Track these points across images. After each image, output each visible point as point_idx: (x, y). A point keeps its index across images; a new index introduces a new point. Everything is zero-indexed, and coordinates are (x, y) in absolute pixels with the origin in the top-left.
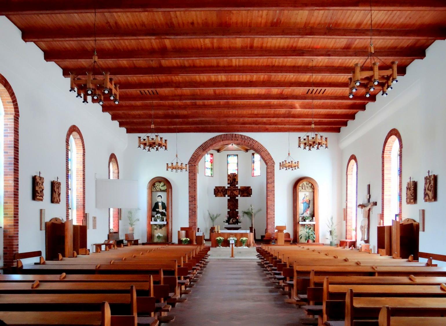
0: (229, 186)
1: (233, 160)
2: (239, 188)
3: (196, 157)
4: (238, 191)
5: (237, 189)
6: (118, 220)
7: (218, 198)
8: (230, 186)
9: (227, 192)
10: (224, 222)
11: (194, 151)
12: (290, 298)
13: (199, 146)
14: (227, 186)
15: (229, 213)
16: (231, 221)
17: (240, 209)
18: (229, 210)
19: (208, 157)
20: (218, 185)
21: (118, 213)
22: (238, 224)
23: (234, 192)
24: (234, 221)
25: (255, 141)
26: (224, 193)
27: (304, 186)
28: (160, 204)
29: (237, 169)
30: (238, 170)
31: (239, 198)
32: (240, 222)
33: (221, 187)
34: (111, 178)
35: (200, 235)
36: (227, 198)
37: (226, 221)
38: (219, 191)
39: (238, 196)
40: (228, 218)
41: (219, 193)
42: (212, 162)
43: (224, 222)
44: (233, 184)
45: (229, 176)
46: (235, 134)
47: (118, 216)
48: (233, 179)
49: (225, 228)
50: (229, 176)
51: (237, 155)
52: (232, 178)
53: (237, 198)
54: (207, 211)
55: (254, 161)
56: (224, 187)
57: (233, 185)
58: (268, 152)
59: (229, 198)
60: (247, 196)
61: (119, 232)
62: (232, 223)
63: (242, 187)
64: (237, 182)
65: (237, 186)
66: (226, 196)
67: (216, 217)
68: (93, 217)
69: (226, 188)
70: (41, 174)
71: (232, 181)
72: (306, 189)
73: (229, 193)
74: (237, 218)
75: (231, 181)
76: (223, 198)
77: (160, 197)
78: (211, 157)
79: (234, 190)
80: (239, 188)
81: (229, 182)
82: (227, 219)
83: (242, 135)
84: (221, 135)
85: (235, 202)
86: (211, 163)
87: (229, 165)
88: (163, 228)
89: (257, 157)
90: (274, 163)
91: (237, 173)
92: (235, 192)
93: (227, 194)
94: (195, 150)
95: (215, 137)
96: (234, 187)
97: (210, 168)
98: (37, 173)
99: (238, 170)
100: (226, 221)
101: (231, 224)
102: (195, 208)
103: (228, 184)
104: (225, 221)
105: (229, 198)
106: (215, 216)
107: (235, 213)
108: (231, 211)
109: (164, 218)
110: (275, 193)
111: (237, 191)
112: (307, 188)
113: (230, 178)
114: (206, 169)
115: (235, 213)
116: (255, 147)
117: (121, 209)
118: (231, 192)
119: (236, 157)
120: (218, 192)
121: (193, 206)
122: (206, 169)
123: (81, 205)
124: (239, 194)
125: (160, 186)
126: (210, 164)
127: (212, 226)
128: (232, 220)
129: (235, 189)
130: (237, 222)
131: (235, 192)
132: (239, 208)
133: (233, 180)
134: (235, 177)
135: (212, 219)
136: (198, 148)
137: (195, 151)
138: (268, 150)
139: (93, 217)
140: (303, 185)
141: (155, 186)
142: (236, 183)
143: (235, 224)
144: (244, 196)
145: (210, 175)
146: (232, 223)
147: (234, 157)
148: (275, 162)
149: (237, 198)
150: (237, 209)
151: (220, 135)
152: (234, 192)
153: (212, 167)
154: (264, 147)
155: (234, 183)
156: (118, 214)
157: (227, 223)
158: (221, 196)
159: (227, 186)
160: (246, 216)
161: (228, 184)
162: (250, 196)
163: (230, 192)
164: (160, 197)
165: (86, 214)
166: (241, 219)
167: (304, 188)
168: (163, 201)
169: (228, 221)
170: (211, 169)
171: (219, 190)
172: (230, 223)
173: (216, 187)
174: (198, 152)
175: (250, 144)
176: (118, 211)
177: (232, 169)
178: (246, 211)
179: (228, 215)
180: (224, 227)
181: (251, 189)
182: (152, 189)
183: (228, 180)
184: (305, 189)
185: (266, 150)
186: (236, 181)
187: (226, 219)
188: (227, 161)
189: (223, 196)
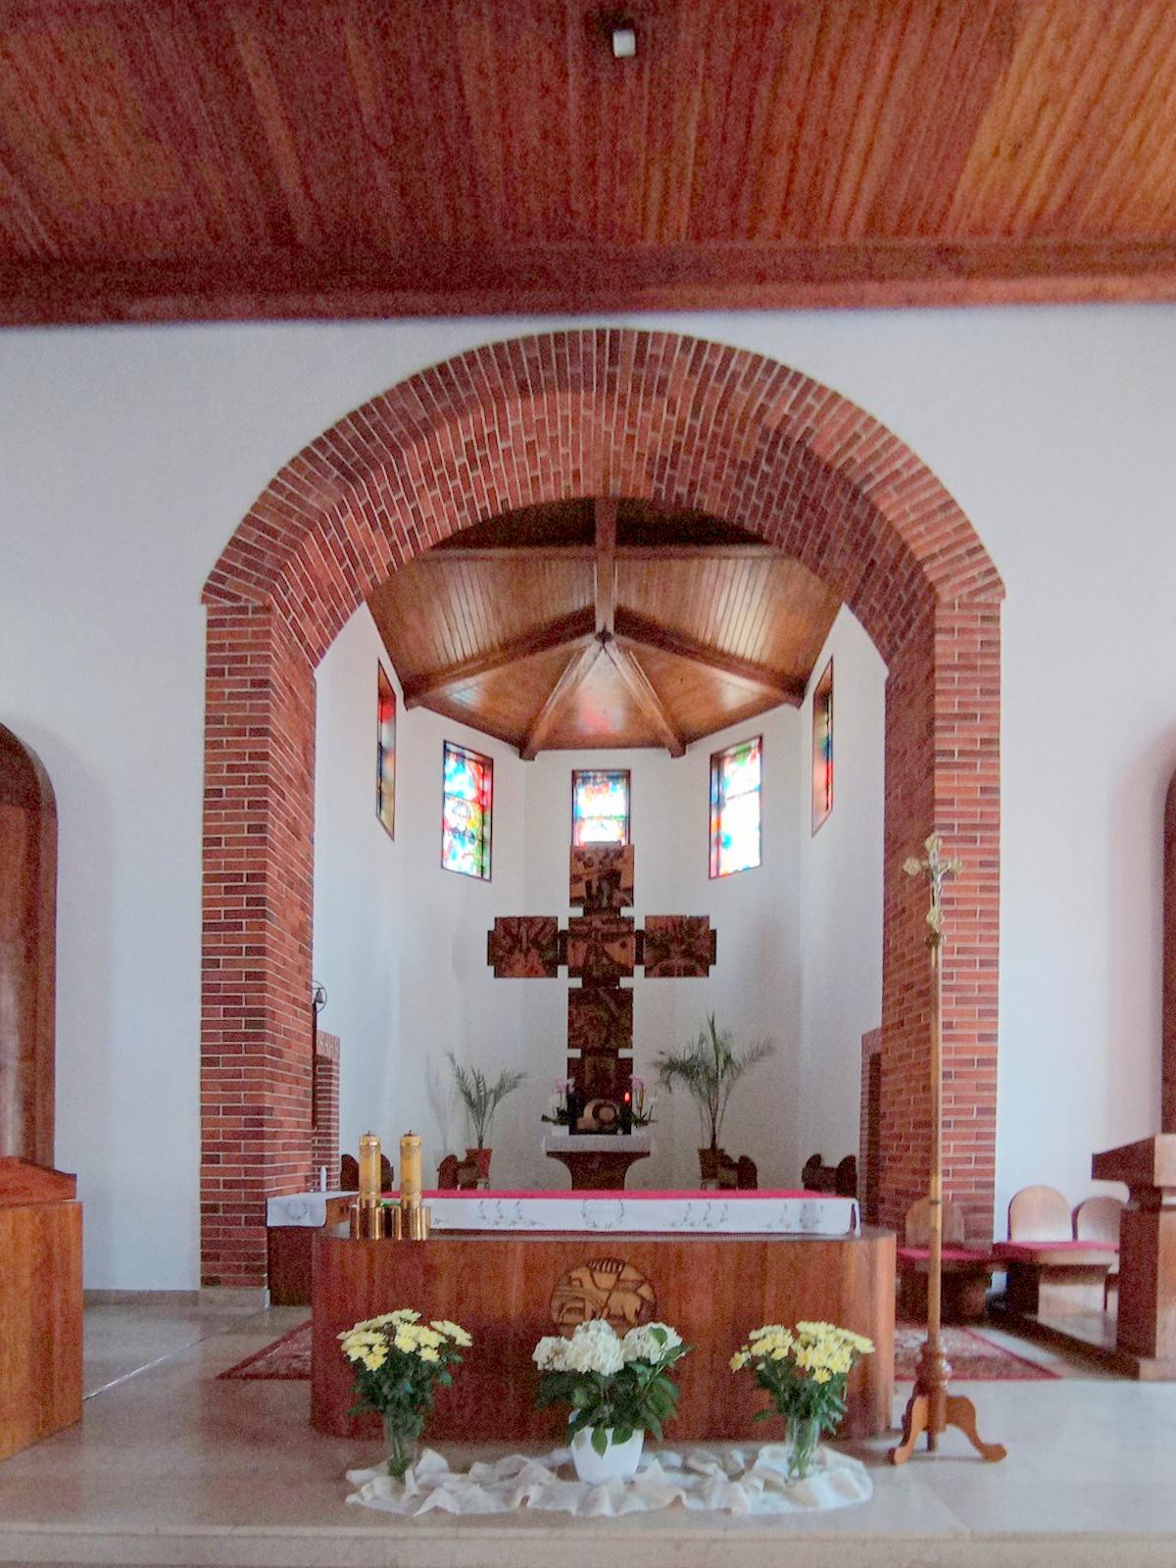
2: (639, 925)
3: (274, 533)
4: (632, 942)
5: (624, 928)
7: (517, 988)
8: (587, 912)
9: (564, 951)
10: (545, 1118)
11: (262, 486)
13: (305, 441)
14: (565, 914)
15: (574, 1067)
16: (588, 1111)
17: (643, 1051)
18: (577, 1053)
20: (516, 910)
22: (627, 1131)
23: (608, 947)
24: (607, 1114)
25: (822, 389)
26: (550, 955)
31: (638, 983)
32: (642, 1122)
33: (531, 921)
35: (306, 1222)
36: (565, 982)
37: (561, 1113)
39: (630, 973)
40: (570, 1099)
42: (485, 804)
43: (545, 1118)
44: (605, 902)
45: (578, 855)
46: (643, 337)
50: (578, 855)
52: (597, 866)
53: (625, 982)
54: (447, 1060)
57: (599, 910)
58: (944, 492)
59: (577, 983)
60: (690, 972)
62: (594, 1125)
63: (656, 918)
64: (630, 890)
65: (625, 912)
66: (563, 970)
67: (498, 1093)
71: (599, 888)
73: (578, 953)
74: (627, 1096)
75: (589, 885)
76: (540, 984)
78: (483, 776)
80: (639, 925)
81: (581, 889)
82: (564, 1106)
83: (702, 344)
84: (513, 345)
85: (613, 1006)
86: (483, 808)
90: (998, 582)
91: (624, 842)
92: (614, 950)
93: (564, 963)
94: (273, 474)
95: (456, 361)
97: (477, 834)
100: (561, 1113)
101: (588, 1132)
104: (554, 1115)
105: (577, 983)
106: (492, 1083)
107: (612, 1073)
110: (1004, 846)
111: (624, 945)
113: (586, 865)
115: (612, 1073)
116: (818, 449)
120: (510, 951)
121: (244, 964)
124: (639, 961)
126: (475, 812)
127: (475, 1146)
128: (596, 1114)
129: (614, 928)
130: (625, 1121)
131: (614, 950)
132: (635, 1038)
133: (600, 879)
134: (619, 865)
135: (471, 1104)
136: (294, 462)
137: (274, 485)
138: (938, 470)
142: (618, 895)
143: (614, 1132)
144: (666, 972)
145: (474, 871)
146: (594, 1125)
148: (1004, 573)
149: (625, 982)
150: (629, 1045)
151: (498, 347)
152: (608, 947)
153: (487, 830)
154: (904, 449)
157: (566, 1129)
158: (531, 973)
159: (565, 914)
160: (679, 1082)
161: (575, 901)
162: (707, 974)
163: (582, 947)
166: (650, 1100)
169: (569, 1117)
170: (483, 841)
171: (517, 939)
172: (581, 1125)
173: (502, 922)
174: (291, 496)
175: (772, 421)
178: (683, 1054)
179: (571, 1081)
180: (544, 1148)
181: (714, 932)
183: (575, 879)
185: (925, 471)
186: (623, 884)
187: (559, 1101)
189: (542, 971)
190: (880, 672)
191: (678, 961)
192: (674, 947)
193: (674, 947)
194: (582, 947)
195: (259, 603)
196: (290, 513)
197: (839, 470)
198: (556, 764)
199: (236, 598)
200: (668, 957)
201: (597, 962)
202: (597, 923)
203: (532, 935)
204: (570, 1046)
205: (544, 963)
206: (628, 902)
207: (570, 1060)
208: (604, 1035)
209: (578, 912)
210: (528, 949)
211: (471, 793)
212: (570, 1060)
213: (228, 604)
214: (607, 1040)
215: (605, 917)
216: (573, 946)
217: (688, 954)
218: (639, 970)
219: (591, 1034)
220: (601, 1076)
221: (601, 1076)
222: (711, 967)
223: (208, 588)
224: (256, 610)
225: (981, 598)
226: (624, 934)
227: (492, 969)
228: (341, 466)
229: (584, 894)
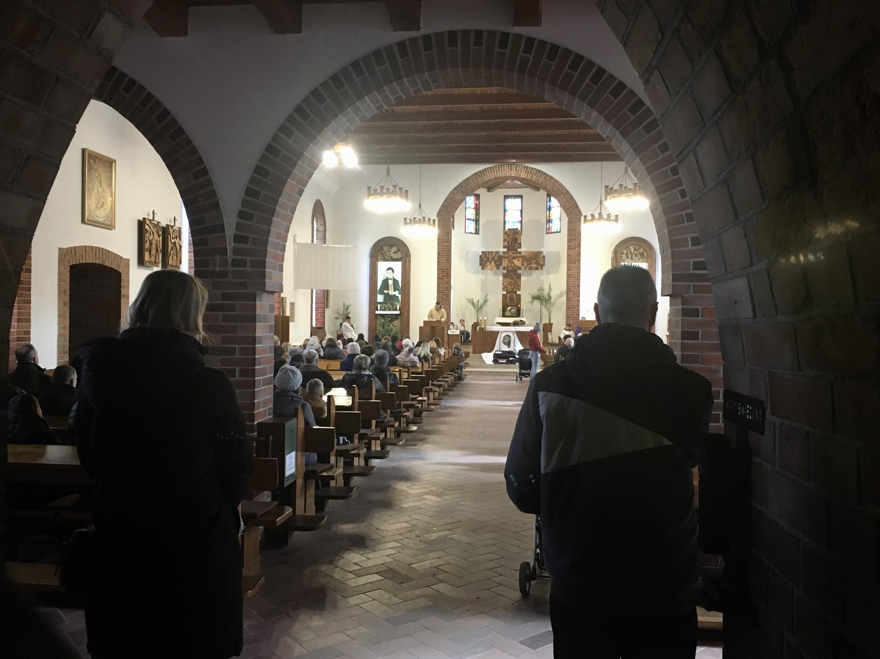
0: (505, 250)
1: (514, 205)
6: (324, 308)
12: (325, 243)
17: (525, 294)
18: (505, 293)
19: (470, 201)
21: (324, 296)
23: (514, 261)
27: (631, 252)
28: (391, 282)
29: (520, 220)
30: (521, 222)
33: (492, 252)
34: (315, 242)
38: (486, 259)
41: (488, 263)
42: (477, 208)
47: (324, 301)
48: (513, 238)
49: (497, 323)
51: (521, 197)
52: (511, 237)
55: (550, 206)
56: (497, 253)
59: (505, 272)
61: (324, 327)
62: (510, 314)
64: (520, 244)
68: (290, 303)
69: (501, 254)
70: (155, 215)
72: (634, 258)
77: (391, 271)
79: (515, 258)
81: (506, 244)
87: (507, 213)
88: (395, 321)
89: (554, 203)
92: (515, 261)
96: (514, 253)
98: (171, 221)
99: (521, 222)
102: (449, 288)
103: (504, 247)
105: (505, 272)
108: (508, 295)
109: (396, 305)
111: (518, 260)
112: (636, 255)
114: (467, 220)
116: (548, 188)
117: (328, 291)
118: (509, 262)
119: (519, 200)
120: (486, 262)
122: (467, 220)
123: (322, 294)
125: (392, 253)
126: (474, 212)
134: (517, 236)
139: (290, 303)
140: (629, 252)
141: (383, 252)
142: (517, 245)
145: (474, 231)
147: (516, 199)
149: (519, 272)
152: (514, 261)
153: (477, 217)
155: (515, 247)
156: (324, 298)
164: (391, 271)
165: (283, 298)
167: (629, 256)
168: (395, 278)
176: (324, 294)
177: (513, 222)
180: (495, 322)
182: (379, 256)
183: (505, 240)
184: (632, 259)
186: (519, 242)
188: (505, 206)
190: (567, 219)
191: (534, 265)
192: (533, 261)
193: (533, 261)
194: (507, 260)
195: (447, 217)
196: (452, 199)
197: (438, 496)
198: (500, 192)
199: (443, 216)
200: (531, 264)
201: (511, 265)
202: (511, 254)
203: (492, 257)
204: (503, 291)
205: (496, 266)
206: (520, 247)
207: (503, 295)
208: (513, 287)
209: (505, 250)
210: (491, 261)
211: (473, 206)
212: (503, 295)
213: (442, 217)
214: (513, 289)
215: (513, 252)
216: (504, 260)
217: (537, 263)
218: (523, 268)
219: (509, 287)
220: (512, 299)
221: (512, 299)
222: (543, 267)
223: (438, 214)
224: (447, 218)
225: (577, 216)
226: (518, 257)
227: (481, 267)
228: (462, 191)
229: (507, 245)
